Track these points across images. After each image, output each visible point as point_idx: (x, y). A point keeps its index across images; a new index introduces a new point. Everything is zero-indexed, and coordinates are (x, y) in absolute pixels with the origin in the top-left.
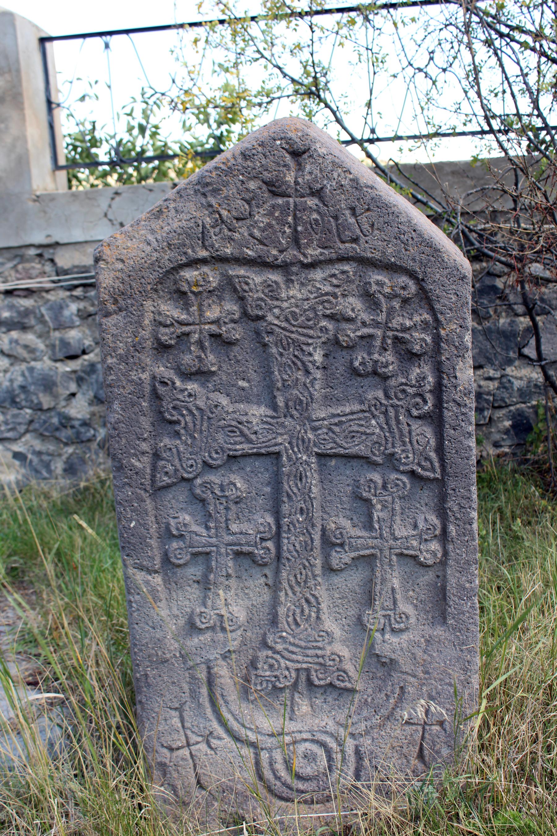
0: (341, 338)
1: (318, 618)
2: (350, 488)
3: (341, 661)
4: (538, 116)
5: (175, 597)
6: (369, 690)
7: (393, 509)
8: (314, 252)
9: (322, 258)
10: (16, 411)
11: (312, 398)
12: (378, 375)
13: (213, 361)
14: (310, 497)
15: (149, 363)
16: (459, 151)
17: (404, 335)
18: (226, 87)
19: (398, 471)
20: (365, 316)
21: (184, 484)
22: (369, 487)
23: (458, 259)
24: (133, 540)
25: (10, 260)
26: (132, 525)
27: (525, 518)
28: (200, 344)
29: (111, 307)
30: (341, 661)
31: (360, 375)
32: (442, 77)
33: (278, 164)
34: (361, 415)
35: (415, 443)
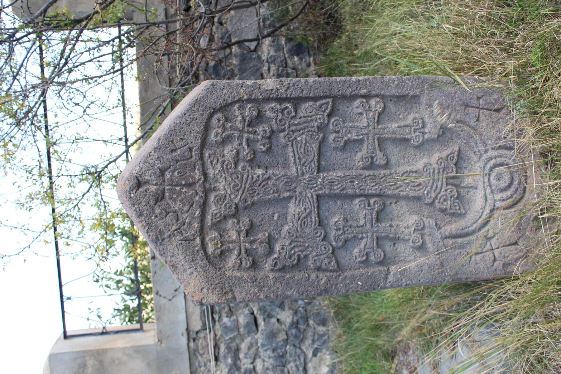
0: (249, 158)
1: (416, 172)
2: (338, 153)
3: (441, 158)
4: (113, 41)
5: (403, 258)
6: (459, 141)
7: (351, 127)
8: (197, 174)
9: (201, 169)
10: (288, 355)
11: (285, 176)
12: (271, 136)
13: (262, 234)
14: (343, 177)
15: (263, 273)
16: (133, 89)
17: (247, 121)
18: (93, 227)
19: (328, 124)
20: (236, 144)
21: (336, 252)
22: (337, 141)
23: (202, 88)
24: (369, 283)
25: (197, 358)
26: (360, 284)
27: (353, 48)
28: (252, 242)
29: (230, 296)
30: (441, 158)
31: (271, 147)
32: (90, 99)
33: (145, 195)
34: (295, 146)
35: (311, 114)
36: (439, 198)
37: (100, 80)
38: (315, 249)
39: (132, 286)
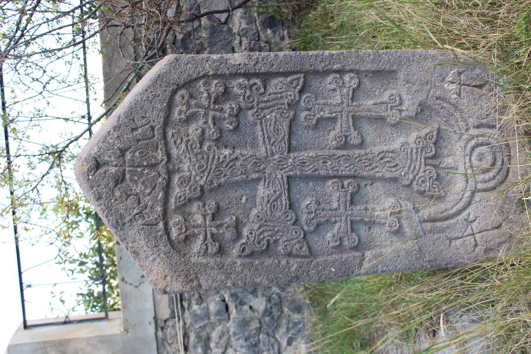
0: (215, 137)
3: (420, 138)
4: (74, 12)
5: (379, 243)
7: (324, 104)
8: (160, 155)
9: (164, 150)
10: (261, 344)
11: (253, 156)
13: (230, 218)
14: (316, 157)
15: (231, 259)
19: (299, 101)
20: (201, 122)
21: (307, 237)
22: (309, 119)
23: (164, 63)
24: (343, 269)
25: (165, 348)
26: (334, 270)
27: (329, 21)
28: (218, 227)
29: (195, 283)
30: (420, 138)
31: (238, 125)
33: (104, 177)
34: (264, 125)
35: (281, 90)
36: (417, 179)
37: (60, 54)
38: (286, 233)
39: (98, 269)
